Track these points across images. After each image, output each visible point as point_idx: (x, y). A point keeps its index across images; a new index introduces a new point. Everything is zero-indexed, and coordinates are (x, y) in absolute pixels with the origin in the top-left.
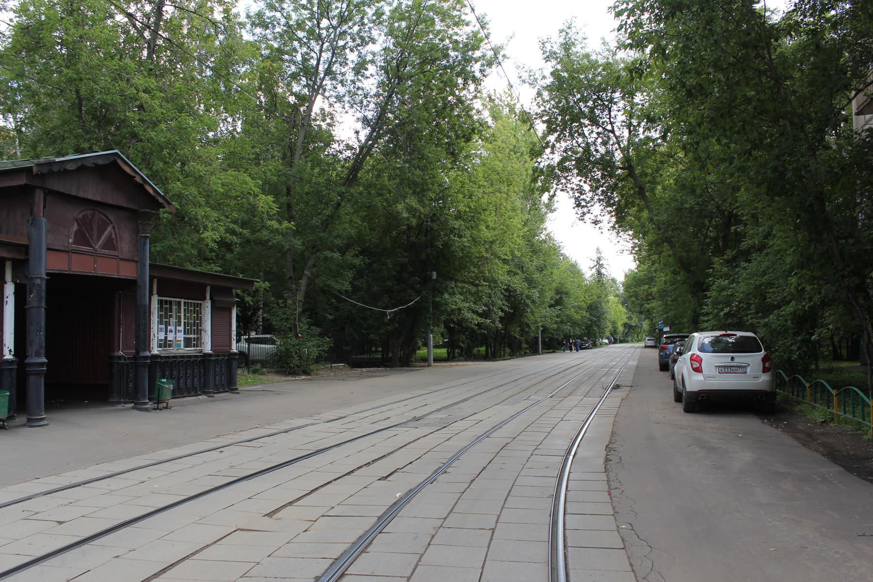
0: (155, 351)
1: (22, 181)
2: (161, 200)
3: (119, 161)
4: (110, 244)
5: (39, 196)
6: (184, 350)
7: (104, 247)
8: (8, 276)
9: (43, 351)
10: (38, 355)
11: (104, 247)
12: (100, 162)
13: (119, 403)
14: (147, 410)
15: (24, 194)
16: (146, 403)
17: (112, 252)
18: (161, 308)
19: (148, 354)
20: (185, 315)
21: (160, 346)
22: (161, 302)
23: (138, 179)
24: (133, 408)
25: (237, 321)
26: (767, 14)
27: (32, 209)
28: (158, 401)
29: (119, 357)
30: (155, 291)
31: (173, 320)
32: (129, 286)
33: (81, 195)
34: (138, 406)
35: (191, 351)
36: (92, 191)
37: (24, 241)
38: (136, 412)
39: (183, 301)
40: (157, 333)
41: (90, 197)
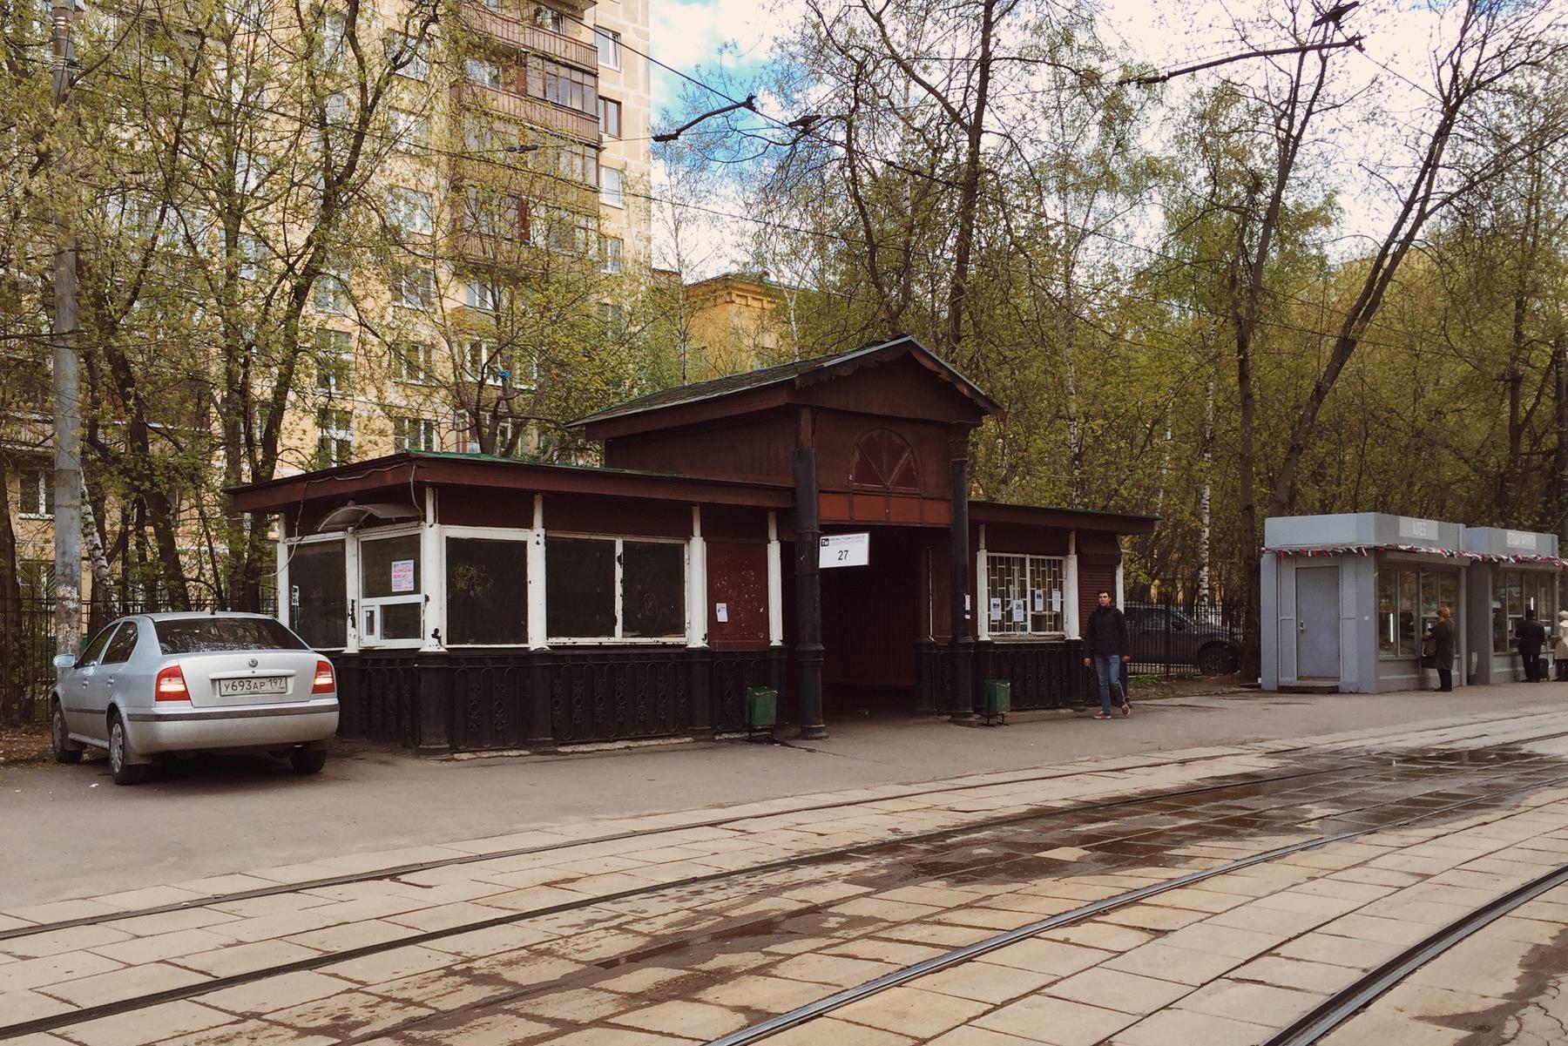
0: (985, 635)
1: (782, 399)
2: (982, 404)
3: (915, 354)
4: (908, 478)
5: (806, 418)
6: (1028, 635)
7: (899, 483)
8: (773, 534)
9: (818, 634)
10: (814, 641)
11: (899, 483)
12: (887, 359)
13: (930, 714)
14: (970, 725)
15: (789, 413)
16: (969, 715)
17: (912, 490)
18: (993, 569)
19: (971, 639)
20: (1032, 580)
21: (992, 628)
22: (992, 561)
23: (944, 375)
24: (950, 721)
25: (292, 582)
26: (886, 146)
27: (797, 436)
28: (989, 717)
29: (931, 645)
30: (982, 545)
31: (1014, 589)
32: (938, 537)
33: (863, 409)
34: (958, 719)
35: (1046, 634)
36: (877, 404)
37: (788, 482)
38: (953, 727)
39: (1028, 557)
40: (986, 611)
41: (875, 411)
